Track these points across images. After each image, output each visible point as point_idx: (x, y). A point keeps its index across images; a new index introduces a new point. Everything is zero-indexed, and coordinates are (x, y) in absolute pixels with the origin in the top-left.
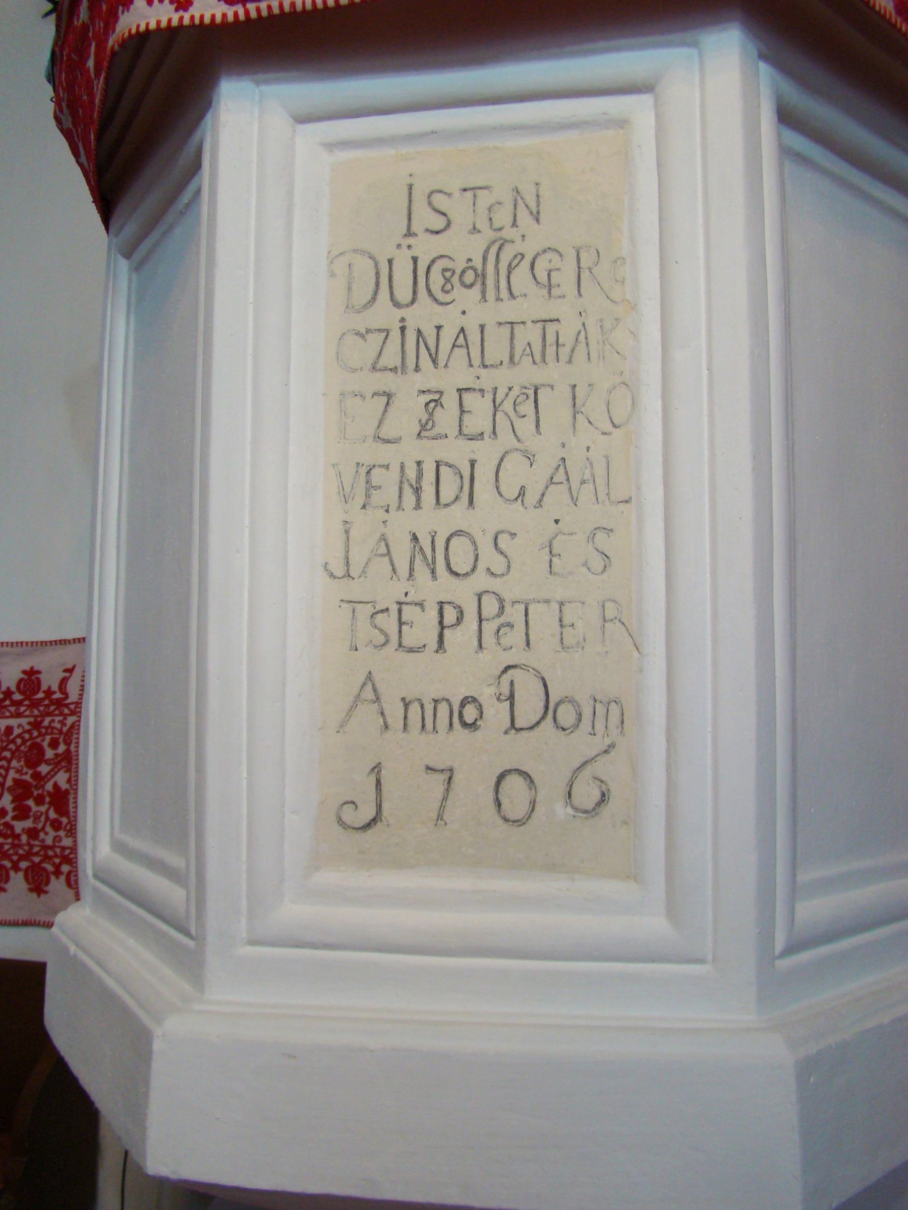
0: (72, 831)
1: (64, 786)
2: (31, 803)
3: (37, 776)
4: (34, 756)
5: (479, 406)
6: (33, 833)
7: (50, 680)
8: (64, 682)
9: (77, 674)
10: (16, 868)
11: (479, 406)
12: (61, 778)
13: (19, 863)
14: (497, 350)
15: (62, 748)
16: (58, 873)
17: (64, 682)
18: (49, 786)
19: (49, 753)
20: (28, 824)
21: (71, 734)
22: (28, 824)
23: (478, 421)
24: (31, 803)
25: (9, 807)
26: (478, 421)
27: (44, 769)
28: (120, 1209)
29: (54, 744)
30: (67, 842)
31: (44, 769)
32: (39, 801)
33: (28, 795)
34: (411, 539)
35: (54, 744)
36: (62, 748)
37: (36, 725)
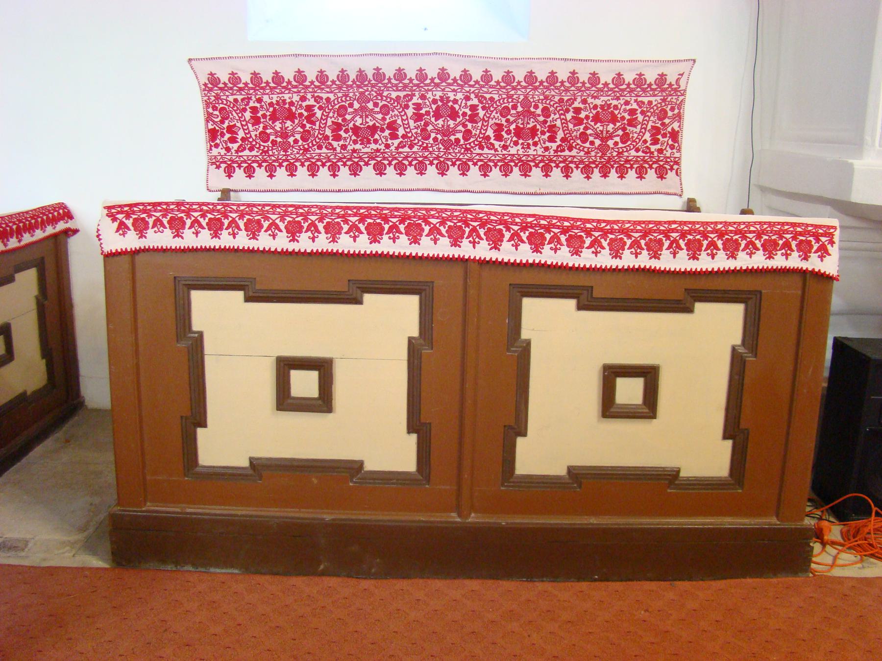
0: (679, 150)
1: (677, 129)
3: (663, 124)
4: (662, 115)
6: (660, 151)
10: (651, 167)
12: (675, 126)
15: (676, 111)
18: (669, 129)
19: (670, 114)
27: (667, 121)
29: (672, 109)
30: (677, 155)
32: (664, 136)
35: (672, 109)
36: (676, 111)
37: (664, 100)
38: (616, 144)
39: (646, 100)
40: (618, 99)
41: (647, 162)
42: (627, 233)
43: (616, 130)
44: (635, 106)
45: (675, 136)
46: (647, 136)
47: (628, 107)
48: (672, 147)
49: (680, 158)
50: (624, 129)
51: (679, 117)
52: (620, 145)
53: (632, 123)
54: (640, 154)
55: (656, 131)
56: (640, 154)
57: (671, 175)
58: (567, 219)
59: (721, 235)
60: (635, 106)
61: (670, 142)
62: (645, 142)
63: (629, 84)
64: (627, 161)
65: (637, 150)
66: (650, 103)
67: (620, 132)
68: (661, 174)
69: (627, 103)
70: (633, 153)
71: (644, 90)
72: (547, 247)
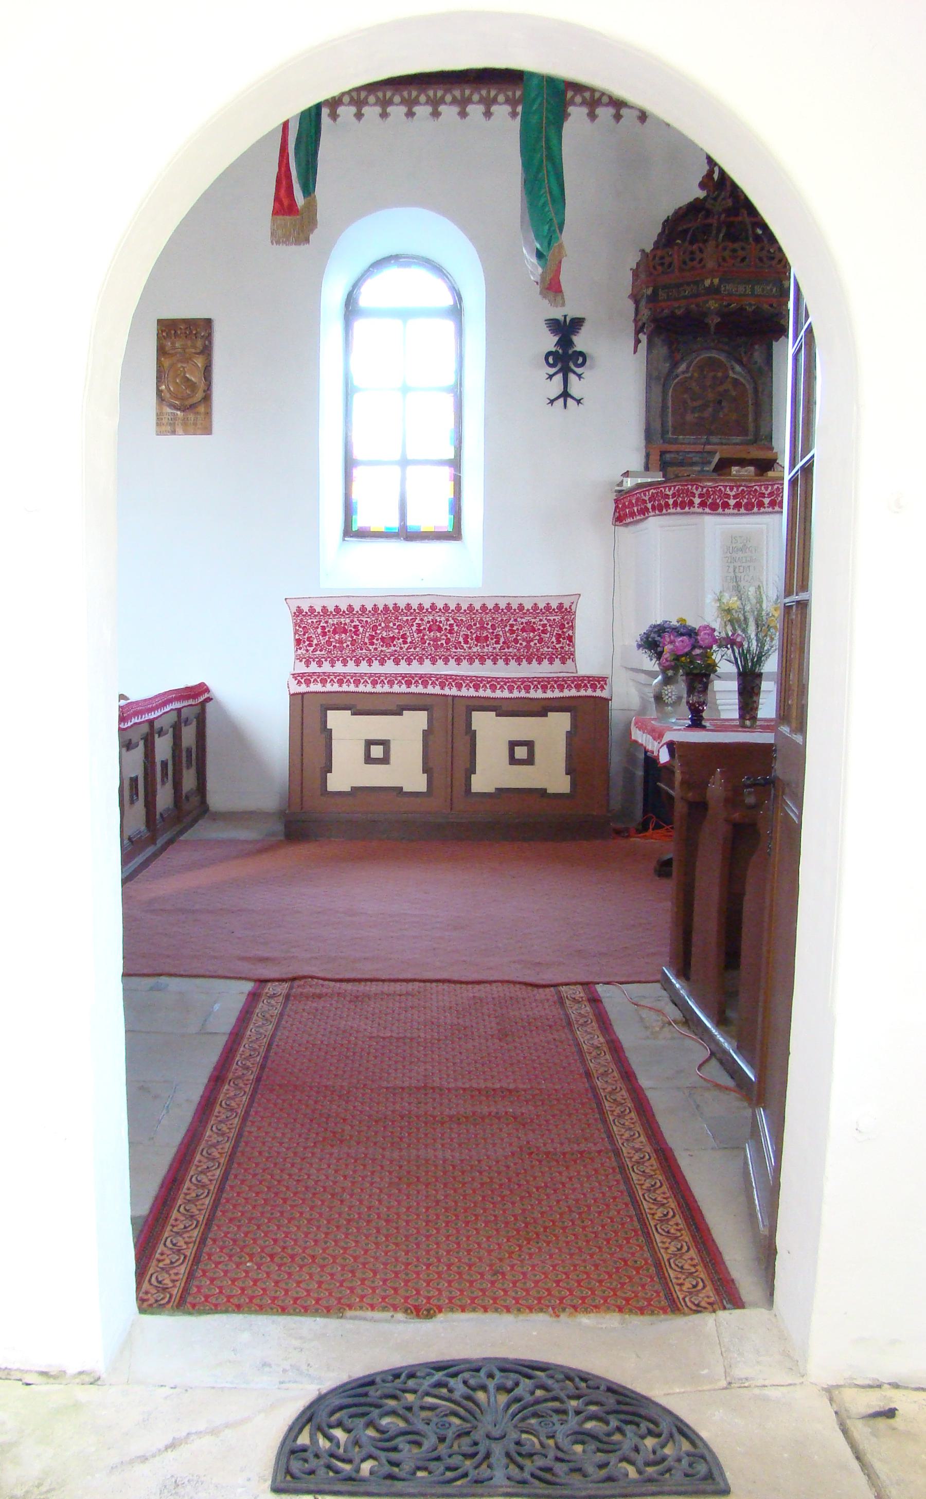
0: (573, 647)
1: (571, 634)
2: (561, 639)
3: (563, 632)
4: (562, 626)
5: (742, 568)
6: (562, 648)
7: (566, 605)
8: (570, 607)
9: (575, 604)
10: (557, 657)
11: (742, 568)
12: (570, 632)
13: (492, 105)
14: (744, 561)
15: (570, 624)
16: (569, 658)
17: (570, 607)
18: (567, 635)
19: (567, 626)
20: (561, 645)
21: (573, 621)
22: (561, 645)
23: (741, 571)
24: (561, 639)
25: (555, 641)
26: (741, 571)
27: (565, 630)
28: (12, 1360)
29: (568, 623)
30: (572, 650)
31: (565, 630)
32: (564, 639)
33: (561, 637)
34: (611, 700)
35: (568, 623)
36: (570, 624)
37: (563, 618)
38: (535, 644)
39: (552, 618)
40: (535, 618)
41: (554, 654)
42: (513, 682)
43: (535, 636)
44: (546, 622)
45: (570, 639)
46: (554, 639)
47: (542, 623)
48: (569, 645)
49: (574, 651)
50: (539, 635)
51: (572, 627)
52: (538, 645)
53: (544, 632)
54: (550, 649)
55: (558, 637)
56: (550, 649)
57: (569, 662)
58: (489, 678)
59: (556, 682)
60: (546, 622)
61: (441, 625)
62: (553, 642)
63: (541, 610)
64: (542, 654)
65: (548, 648)
66: (554, 620)
67: (537, 637)
68: (563, 661)
69: (541, 620)
70: (546, 649)
71: (551, 613)
72: (481, 689)
